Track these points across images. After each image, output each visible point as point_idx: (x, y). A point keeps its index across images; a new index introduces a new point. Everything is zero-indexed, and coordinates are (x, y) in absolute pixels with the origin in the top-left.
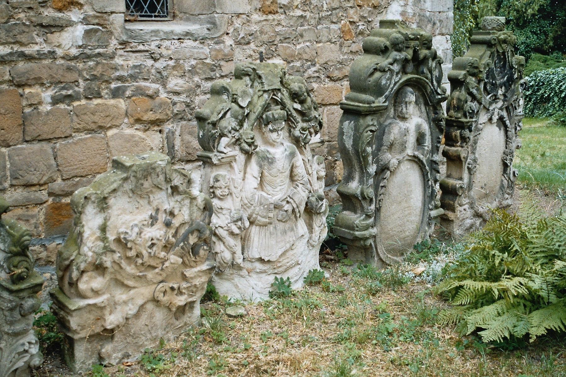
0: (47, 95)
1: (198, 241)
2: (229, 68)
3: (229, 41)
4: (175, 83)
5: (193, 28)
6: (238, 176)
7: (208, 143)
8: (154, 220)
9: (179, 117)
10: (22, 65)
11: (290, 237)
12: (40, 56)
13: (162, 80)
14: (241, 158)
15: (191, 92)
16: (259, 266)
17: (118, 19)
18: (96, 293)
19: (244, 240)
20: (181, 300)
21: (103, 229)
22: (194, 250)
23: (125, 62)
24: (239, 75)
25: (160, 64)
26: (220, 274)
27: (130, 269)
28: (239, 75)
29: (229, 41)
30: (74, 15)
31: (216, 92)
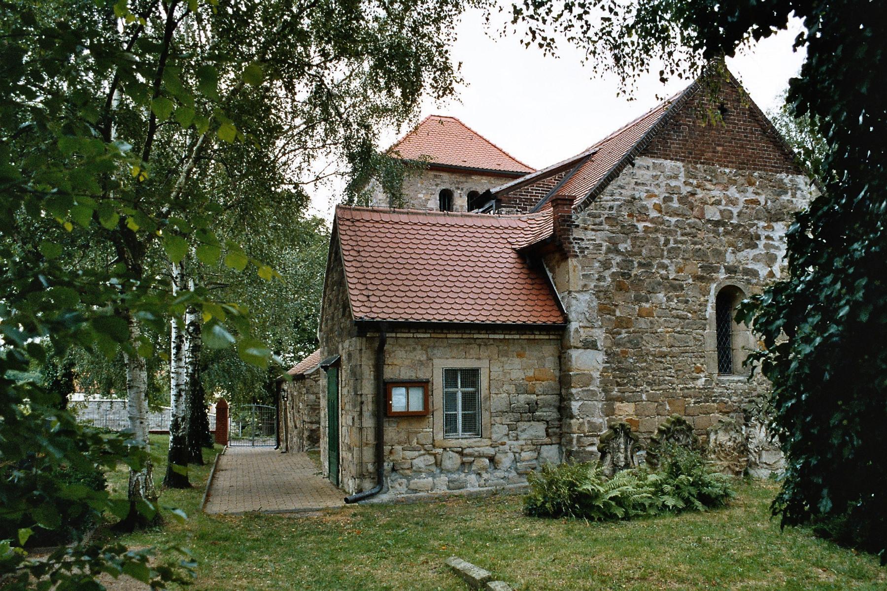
0: (693, 401)
1: (743, 449)
2: (755, 393)
3: (755, 383)
4: (734, 398)
5: (741, 378)
6: (758, 431)
7: (747, 419)
8: (730, 440)
9: (735, 411)
10: (686, 391)
11: (778, 457)
12: (692, 388)
13: (730, 397)
14: (759, 425)
15: (740, 402)
16: (765, 466)
17: (716, 376)
18: (712, 459)
19: (760, 456)
20: (737, 469)
21: (716, 439)
22: (742, 452)
23: (718, 391)
24: (759, 396)
25: (729, 392)
26: (750, 466)
27: (723, 454)
28: (759, 396)
29: (755, 383)
30: (702, 375)
31: (750, 402)
